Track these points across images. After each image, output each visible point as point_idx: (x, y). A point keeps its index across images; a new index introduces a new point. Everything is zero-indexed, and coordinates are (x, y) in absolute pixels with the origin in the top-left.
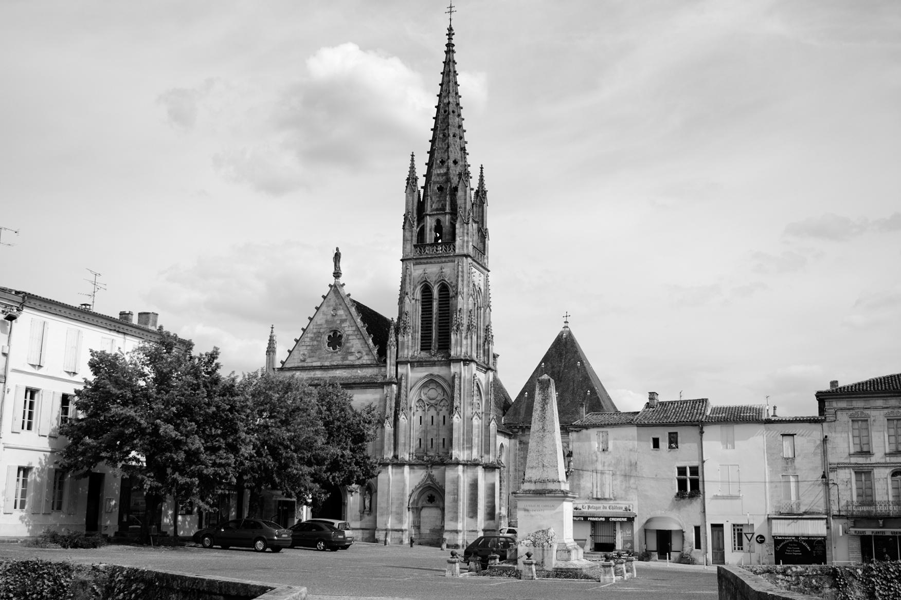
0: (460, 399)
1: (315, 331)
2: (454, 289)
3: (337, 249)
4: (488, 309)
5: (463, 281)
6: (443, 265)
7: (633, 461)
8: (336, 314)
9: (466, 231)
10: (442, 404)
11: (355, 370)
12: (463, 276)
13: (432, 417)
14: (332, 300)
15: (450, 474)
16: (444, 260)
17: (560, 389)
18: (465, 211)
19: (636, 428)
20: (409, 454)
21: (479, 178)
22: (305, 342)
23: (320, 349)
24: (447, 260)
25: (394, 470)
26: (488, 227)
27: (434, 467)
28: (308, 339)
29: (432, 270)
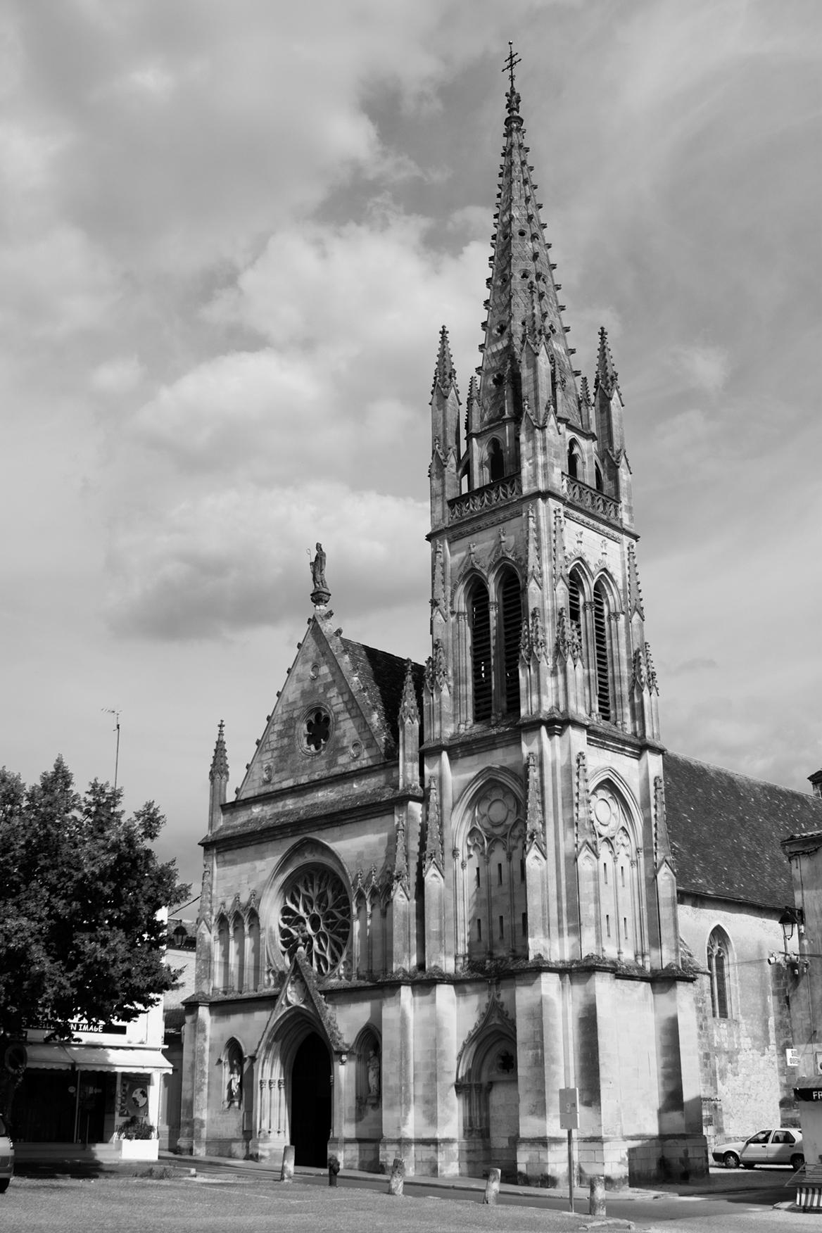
0: (543, 812)
1: (285, 717)
4: (636, 617)
5: (538, 549)
6: (500, 527)
8: (318, 676)
9: (539, 444)
12: (538, 540)
13: (500, 865)
14: (311, 649)
15: (523, 997)
16: (501, 515)
17: (515, 669)
18: (537, 404)
20: (456, 958)
22: (269, 742)
23: (294, 752)
24: (507, 513)
25: (418, 999)
27: (503, 982)
29: (482, 546)
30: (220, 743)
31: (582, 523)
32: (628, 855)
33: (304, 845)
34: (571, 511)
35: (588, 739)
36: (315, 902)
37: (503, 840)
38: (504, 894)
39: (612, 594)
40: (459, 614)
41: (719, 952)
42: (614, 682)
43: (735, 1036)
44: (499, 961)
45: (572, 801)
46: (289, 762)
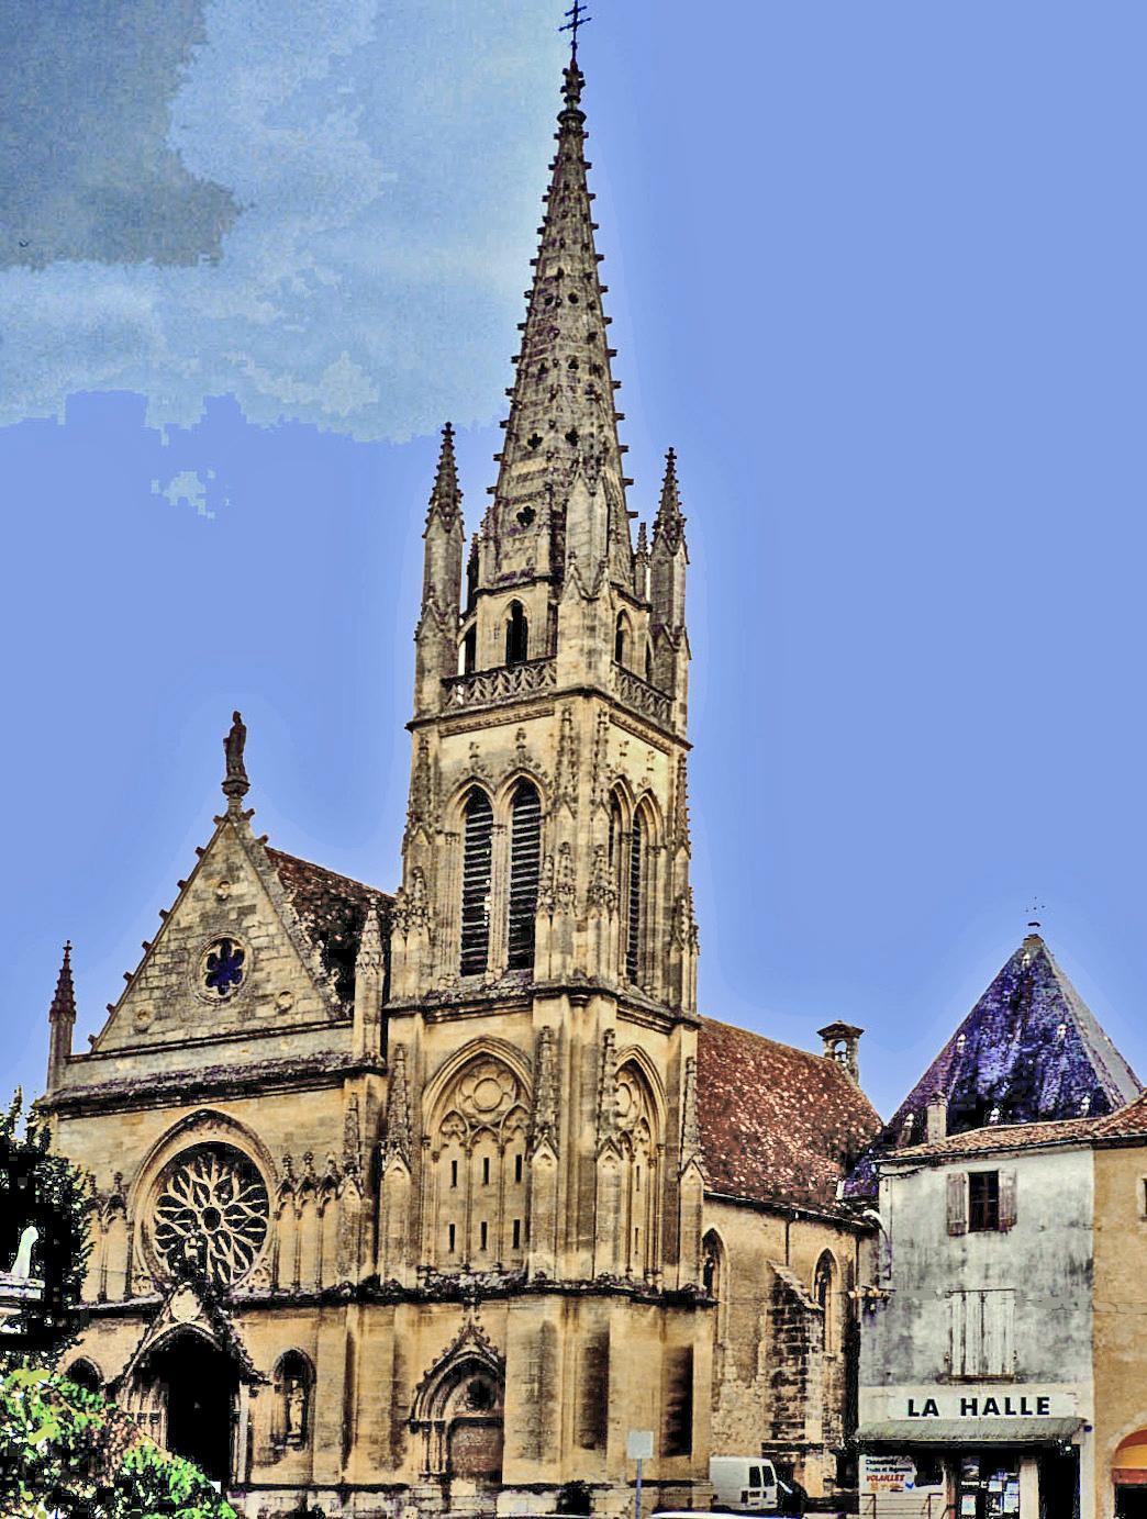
2: (550, 792)
3: (237, 716)
7: (1081, 1258)
10: (513, 1123)
11: (273, 1042)
16: (523, 711)
19: (1090, 1154)
21: (662, 485)
22: (147, 978)
28: (155, 972)
30: (66, 972)
32: (645, 1153)
33: (201, 1119)
34: (617, 713)
35: (619, 1012)
36: (213, 1194)
37: (495, 1130)
38: (491, 1196)
39: (654, 823)
40: (453, 835)
41: (709, 1261)
42: (645, 937)
43: (720, 1363)
44: (478, 1277)
45: (595, 1089)
46: (178, 1007)
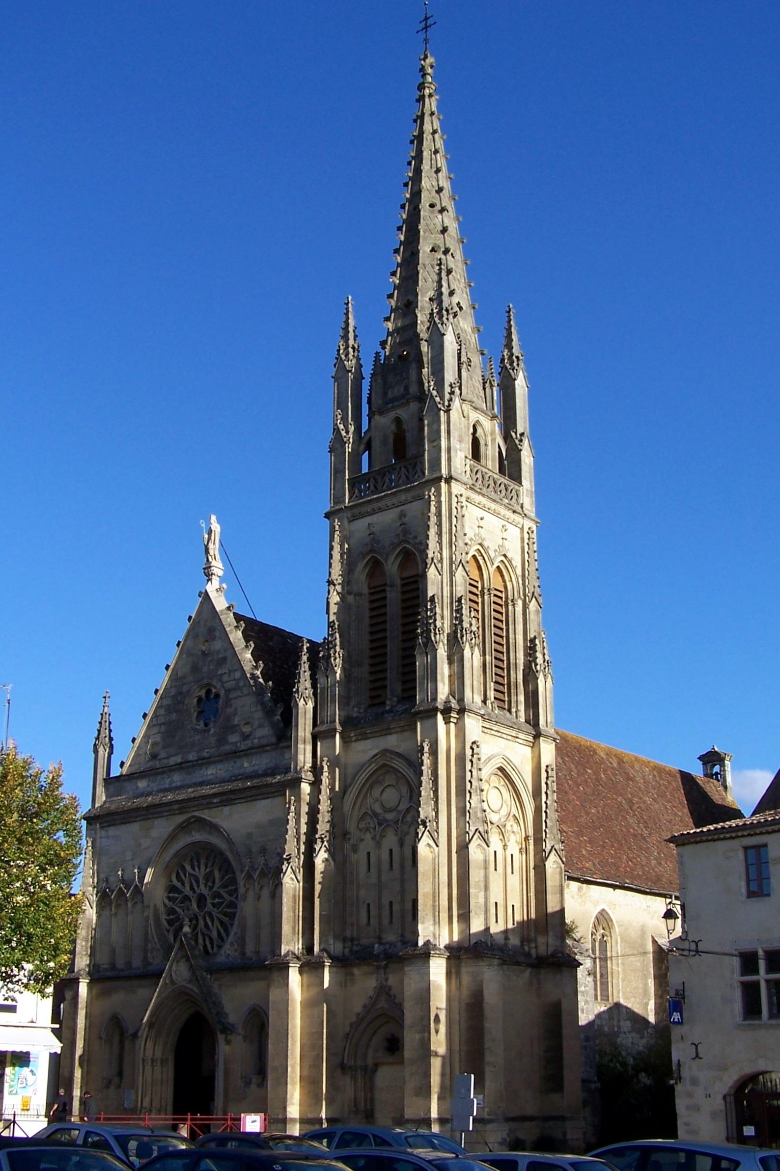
13: (391, 851)
26: (677, 768)
31: (483, 508)
